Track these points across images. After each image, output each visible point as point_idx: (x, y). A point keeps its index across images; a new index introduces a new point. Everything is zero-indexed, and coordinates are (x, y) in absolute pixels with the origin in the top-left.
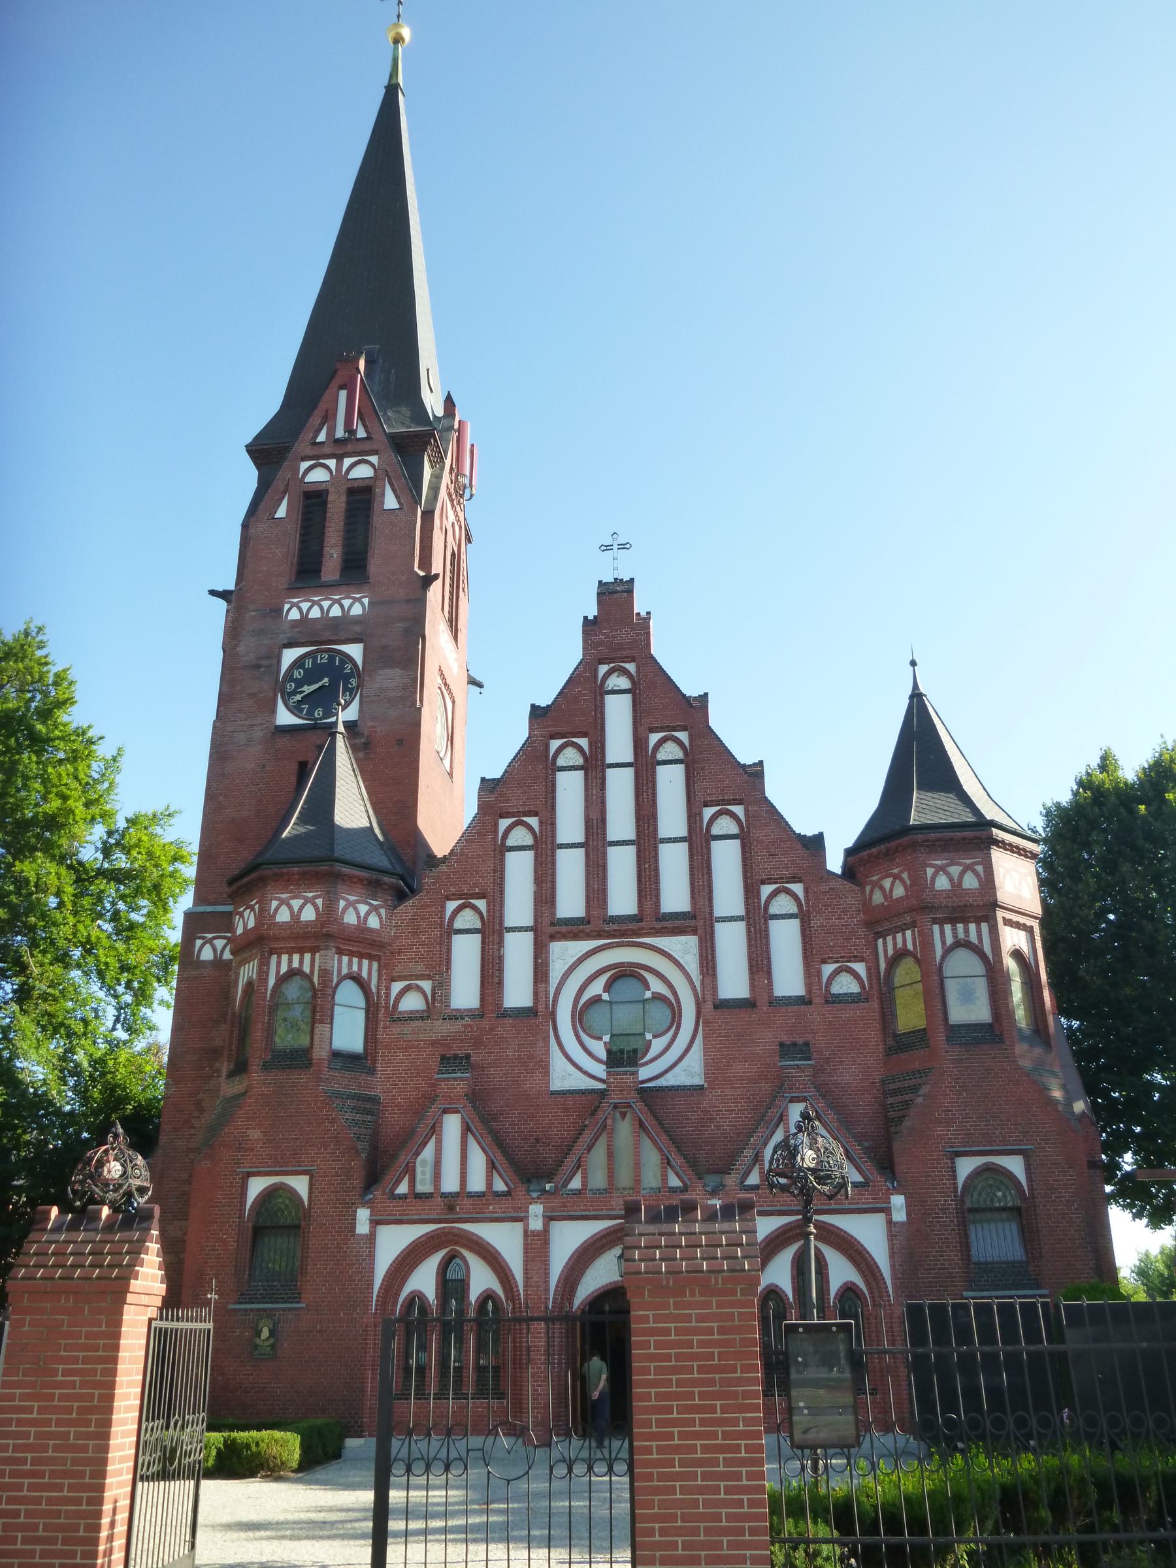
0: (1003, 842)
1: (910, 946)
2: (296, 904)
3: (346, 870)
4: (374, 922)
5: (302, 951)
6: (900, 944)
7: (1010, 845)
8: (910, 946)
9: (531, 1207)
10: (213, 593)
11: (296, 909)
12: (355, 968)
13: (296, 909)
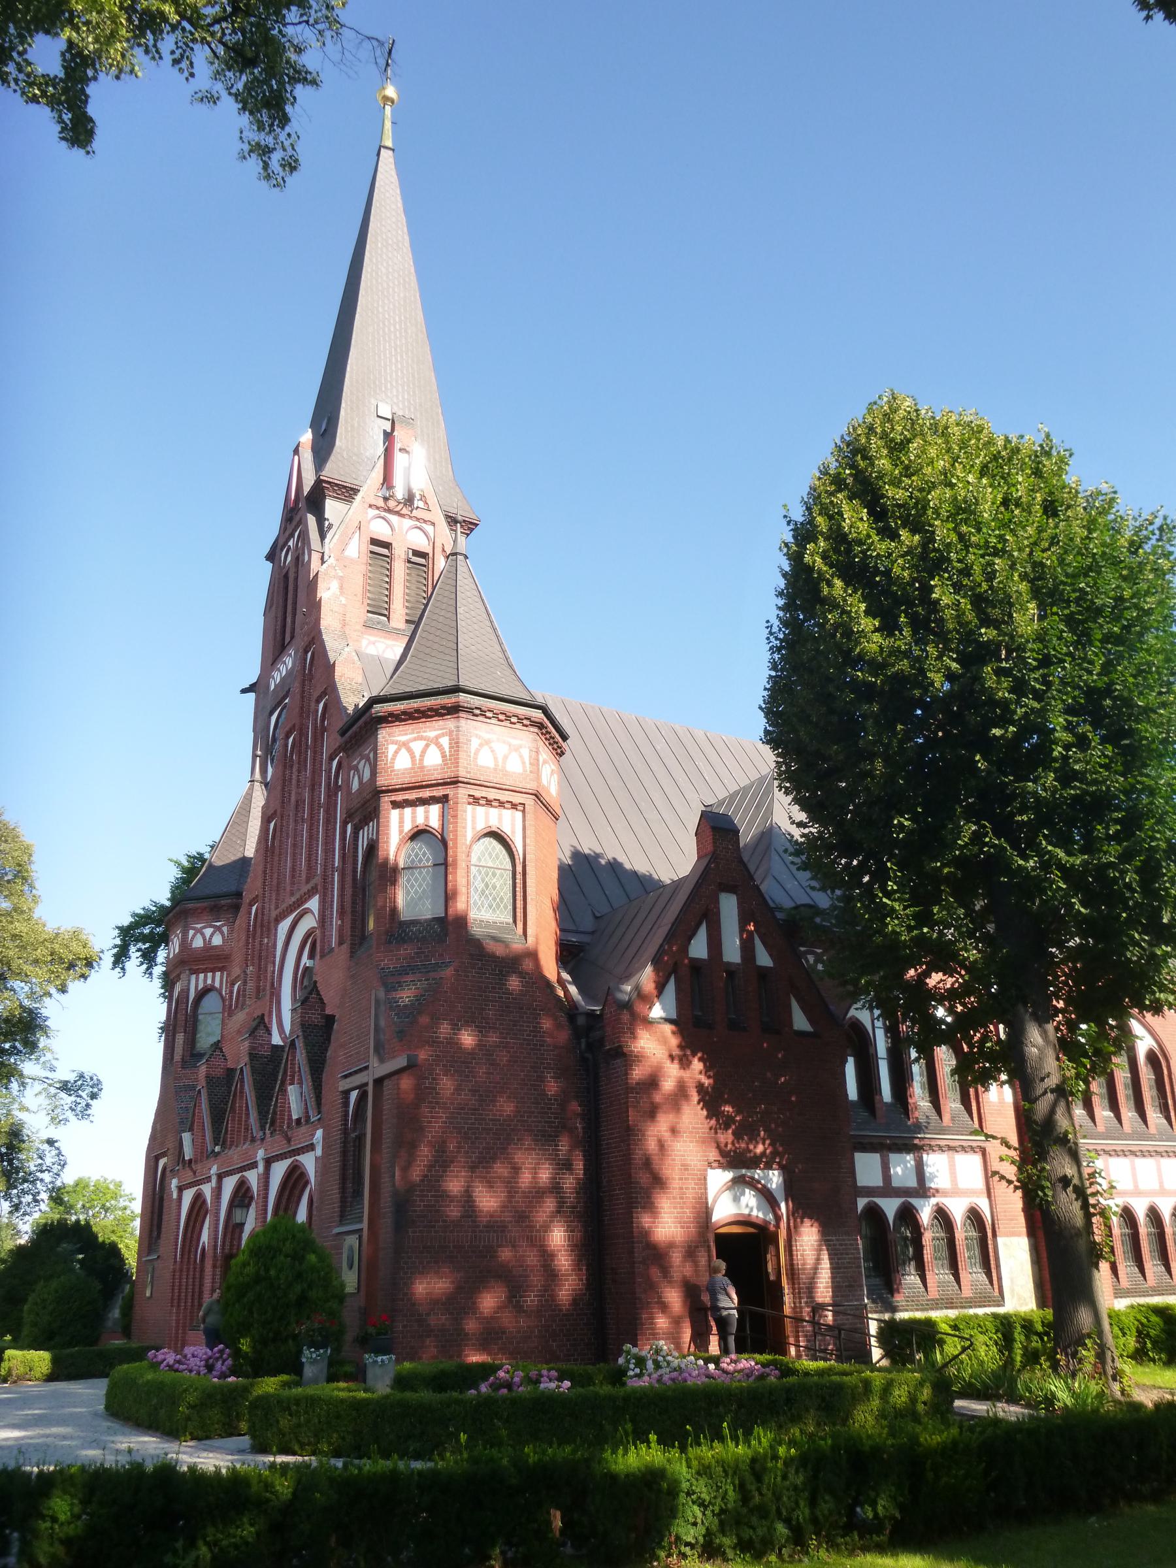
0: (391, 714)
1: (217, 985)
2: (208, 932)
3: (190, 905)
4: (217, 941)
5: (213, 971)
6: (209, 982)
8: (217, 985)
9: (776, 1172)
10: (244, 691)
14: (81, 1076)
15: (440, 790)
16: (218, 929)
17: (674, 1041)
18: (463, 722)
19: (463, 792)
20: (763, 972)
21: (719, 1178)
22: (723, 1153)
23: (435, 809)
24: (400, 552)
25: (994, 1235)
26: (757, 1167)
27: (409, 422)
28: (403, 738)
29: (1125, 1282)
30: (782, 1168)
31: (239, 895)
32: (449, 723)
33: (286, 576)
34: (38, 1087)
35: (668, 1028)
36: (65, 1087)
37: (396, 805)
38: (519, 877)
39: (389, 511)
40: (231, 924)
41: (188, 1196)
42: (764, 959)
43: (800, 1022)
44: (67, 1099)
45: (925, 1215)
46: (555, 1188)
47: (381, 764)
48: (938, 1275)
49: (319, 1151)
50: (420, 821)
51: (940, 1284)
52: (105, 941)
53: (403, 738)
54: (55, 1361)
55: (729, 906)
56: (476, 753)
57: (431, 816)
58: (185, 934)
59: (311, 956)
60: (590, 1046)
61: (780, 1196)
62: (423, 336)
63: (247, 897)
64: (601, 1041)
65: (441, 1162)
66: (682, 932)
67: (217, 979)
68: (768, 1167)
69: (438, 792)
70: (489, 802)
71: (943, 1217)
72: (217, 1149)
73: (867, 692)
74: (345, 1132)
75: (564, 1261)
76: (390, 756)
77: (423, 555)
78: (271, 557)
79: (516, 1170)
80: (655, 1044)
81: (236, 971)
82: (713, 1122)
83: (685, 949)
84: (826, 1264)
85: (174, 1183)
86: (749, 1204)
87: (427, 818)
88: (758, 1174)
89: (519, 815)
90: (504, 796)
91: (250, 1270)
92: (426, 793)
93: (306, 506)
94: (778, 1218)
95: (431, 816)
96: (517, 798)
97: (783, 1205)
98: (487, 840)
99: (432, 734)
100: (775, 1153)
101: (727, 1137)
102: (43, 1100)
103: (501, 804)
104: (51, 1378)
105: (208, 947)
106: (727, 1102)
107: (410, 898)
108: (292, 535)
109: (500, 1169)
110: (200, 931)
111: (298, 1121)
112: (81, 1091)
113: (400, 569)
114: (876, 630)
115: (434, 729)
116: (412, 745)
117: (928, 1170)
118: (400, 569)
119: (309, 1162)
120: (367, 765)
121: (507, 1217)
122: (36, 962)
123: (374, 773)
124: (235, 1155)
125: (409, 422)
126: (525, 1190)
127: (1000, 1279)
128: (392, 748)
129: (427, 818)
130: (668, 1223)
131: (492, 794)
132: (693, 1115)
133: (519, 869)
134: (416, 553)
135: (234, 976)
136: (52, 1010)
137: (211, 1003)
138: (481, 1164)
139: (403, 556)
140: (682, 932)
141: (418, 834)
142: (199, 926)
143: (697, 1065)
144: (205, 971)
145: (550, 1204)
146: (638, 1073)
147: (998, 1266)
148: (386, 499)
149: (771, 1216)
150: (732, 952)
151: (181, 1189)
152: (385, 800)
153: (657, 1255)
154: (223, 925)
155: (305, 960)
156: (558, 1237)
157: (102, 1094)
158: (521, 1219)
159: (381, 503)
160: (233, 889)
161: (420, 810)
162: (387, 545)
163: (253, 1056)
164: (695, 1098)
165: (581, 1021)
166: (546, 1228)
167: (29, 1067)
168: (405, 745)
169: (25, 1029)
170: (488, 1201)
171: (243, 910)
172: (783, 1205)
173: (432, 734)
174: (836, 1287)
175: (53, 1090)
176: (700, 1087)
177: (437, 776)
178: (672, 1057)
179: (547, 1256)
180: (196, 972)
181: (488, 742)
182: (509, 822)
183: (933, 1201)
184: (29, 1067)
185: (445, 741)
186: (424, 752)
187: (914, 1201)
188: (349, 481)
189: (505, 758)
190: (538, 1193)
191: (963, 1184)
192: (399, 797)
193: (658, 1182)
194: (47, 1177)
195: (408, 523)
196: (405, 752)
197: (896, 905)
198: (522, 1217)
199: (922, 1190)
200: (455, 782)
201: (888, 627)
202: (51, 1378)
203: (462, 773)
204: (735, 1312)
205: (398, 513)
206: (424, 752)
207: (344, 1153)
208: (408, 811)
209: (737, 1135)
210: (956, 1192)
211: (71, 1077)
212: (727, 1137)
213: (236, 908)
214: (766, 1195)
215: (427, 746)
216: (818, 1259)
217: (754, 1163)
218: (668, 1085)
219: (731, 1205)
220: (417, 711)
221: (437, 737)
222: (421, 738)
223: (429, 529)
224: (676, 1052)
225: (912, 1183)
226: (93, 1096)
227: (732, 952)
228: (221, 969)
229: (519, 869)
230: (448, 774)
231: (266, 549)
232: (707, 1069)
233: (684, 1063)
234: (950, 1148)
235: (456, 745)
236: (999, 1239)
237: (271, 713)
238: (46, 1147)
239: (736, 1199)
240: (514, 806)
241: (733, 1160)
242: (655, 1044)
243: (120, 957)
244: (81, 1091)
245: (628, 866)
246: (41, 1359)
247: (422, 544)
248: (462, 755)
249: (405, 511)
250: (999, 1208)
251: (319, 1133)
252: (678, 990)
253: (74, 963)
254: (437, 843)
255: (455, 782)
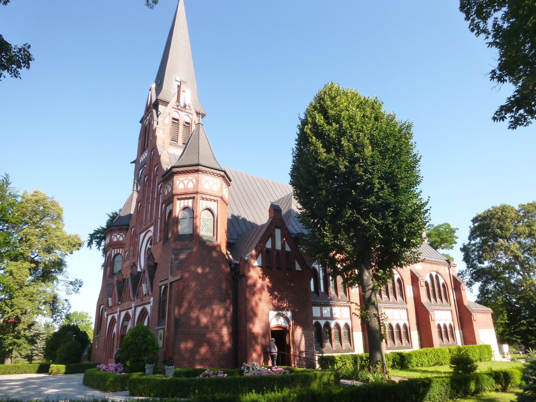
0: (178, 172)
2: (118, 236)
3: (113, 228)
4: (121, 239)
5: (120, 248)
7: (182, 171)
8: (121, 252)
10: (132, 163)
14: (77, 280)
15: (192, 195)
16: (122, 235)
17: (260, 273)
18: (200, 175)
19: (199, 196)
20: (287, 253)
21: (273, 314)
22: (274, 306)
23: (190, 201)
24: (181, 122)
25: (410, 331)
26: (284, 310)
27: (185, 83)
28: (182, 179)
29: (389, 346)
30: (291, 311)
31: (128, 225)
32: (196, 175)
33: (146, 128)
34: (63, 283)
35: (259, 269)
36: (71, 283)
37: (179, 199)
38: (215, 222)
39: (178, 109)
40: (126, 234)
41: (110, 317)
42: (288, 249)
43: (298, 268)
44: (72, 287)
45: (332, 325)
46: (225, 316)
47: (174, 187)
48: (336, 343)
49: (152, 304)
50: (186, 204)
51: (336, 346)
52: (85, 238)
53: (182, 179)
54: (67, 368)
55: (278, 232)
56: (204, 184)
57: (189, 203)
58: (111, 237)
59: (151, 244)
60: (235, 274)
61: (290, 319)
62: (191, 57)
63: (131, 226)
64: (239, 272)
65: (190, 308)
66: (264, 240)
67: (121, 251)
68: (287, 310)
69: (192, 196)
70: (207, 199)
71: (337, 326)
72: (120, 303)
73: (321, 170)
74: (160, 298)
75: (226, 338)
76: (177, 184)
77: (189, 124)
78: (141, 122)
79: (213, 311)
80: (255, 273)
81: (127, 249)
82: (271, 297)
83: (265, 245)
84: (303, 339)
85: (106, 313)
86: (281, 322)
87: (188, 203)
88: (284, 312)
89: (216, 203)
90: (212, 198)
91: (130, 340)
92: (188, 196)
93: (153, 107)
94: (290, 326)
95: (189, 203)
96: (215, 198)
97: (291, 322)
98: (206, 211)
99: (190, 178)
100: (289, 306)
101: (275, 302)
102: (64, 287)
103: (211, 200)
104: (66, 373)
105: (118, 241)
106: (275, 291)
107: (183, 228)
108: (148, 116)
109: (208, 310)
110: (116, 236)
111: (145, 295)
112: (77, 284)
113: (181, 127)
114: (325, 152)
115: (191, 177)
117: (334, 312)
118: (181, 127)
119: (148, 307)
121: (210, 325)
122: (63, 244)
123: (172, 189)
124: (125, 305)
125: (185, 83)
126: (213, 318)
127: (353, 344)
128: (178, 182)
129: (188, 203)
130: (257, 328)
131: (208, 197)
132: (266, 295)
133: (216, 220)
134: (186, 123)
135: (126, 249)
136: (68, 259)
137: (118, 258)
138: (202, 308)
139: (182, 124)
140: (264, 240)
141: (185, 208)
143: (267, 280)
144: (117, 248)
145: (223, 321)
146: (250, 282)
147: (353, 341)
148: (178, 106)
149: (287, 325)
150: (278, 247)
151: (107, 315)
152: (175, 198)
153: (254, 337)
155: (149, 246)
156: (225, 331)
157: (83, 286)
158: (213, 326)
159: (176, 107)
160: (126, 223)
161: (186, 201)
162: (177, 120)
163: (132, 275)
164: (266, 290)
165: (233, 266)
166: (221, 328)
167: (60, 277)
168: (182, 181)
169: (59, 265)
170: (204, 320)
171: (129, 230)
172: (291, 322)
173: (190, 178)
174: (306, 346)
175: (67, 284)
176: (268, 287)
177: (191, 191)
178: (260, 277)
179: (221, 337)
180: (114, 249)
181: (207, 181)
182: (213, 205)
183: (335, 321)
184: (60, 277)
185: (194, 180)
186: (188, 184)
187: (329, 321)
188: (166, 99)
189: (213, 186)
190: (219, 318)
191: (343, 316)
192: (180, 197)
193: (255, 314)
194: (65, 311)
195: (184, 113)
196: (182, 183)
197: (328, 234)
198: (214, 325)
199: (332, 318)
200: (197, 193)
201: (328, 152)
202: (66, 373)
203: (199, 190)
204: (276, 354)
205: (181, 110)
206: (188, 184)
207: (160, 304)
208: (182, 201)
209: (279, 301)
210: (341, 319)
211: (73, 280)
212: (275, 302)
213: (127, 229)
214: (286, 319)
216: (301, 338)
217: (283, 309)
218: (259, 286)
219: (276, 321)
220: (186, 171)
222: (187, 179)
223: (191, 116)
224: (261, 276)
225: (329, 316)
226: (80, 286)
227: (278, 247)
228: (122, 248)
229: (216, 220)
230: (195, 190)
231: (140, 119)
232: (270, 281)
233: (263, 279)
234: (340, 306)
235: (197, 182)
236: (354, 333)
237: (140, 170)
238: (65, 302)
239: (277, 320)
240: (215, 201)
241: (277, 308)
242: (255, 273)
243: (90, 243)
244: (77, 284)
245: (248, 220)
246: (62, 367)
247: (188, 120)
248: (199, 185)
249: (183, 110)
250: (354, 323)
251: (152, 299)
252: (262, 257)
253: (74, 245)
254: (191, 211)
255: (197, 193)
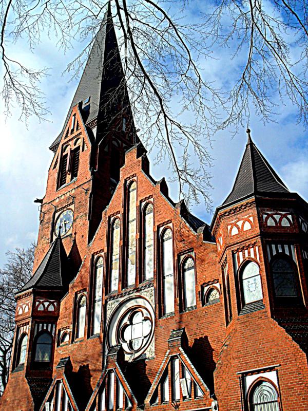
2: (46, 304)
11: (240, 226)
12: (280, 251)
13: (240, 226)
16: (52, 303)
116: (45, 303)
120: (27, 306)
142: (41, 300)
154: (55, 302)
186: (243, 226)
215: (244, 223)
221: (53, 302)
222: (48, 301)
